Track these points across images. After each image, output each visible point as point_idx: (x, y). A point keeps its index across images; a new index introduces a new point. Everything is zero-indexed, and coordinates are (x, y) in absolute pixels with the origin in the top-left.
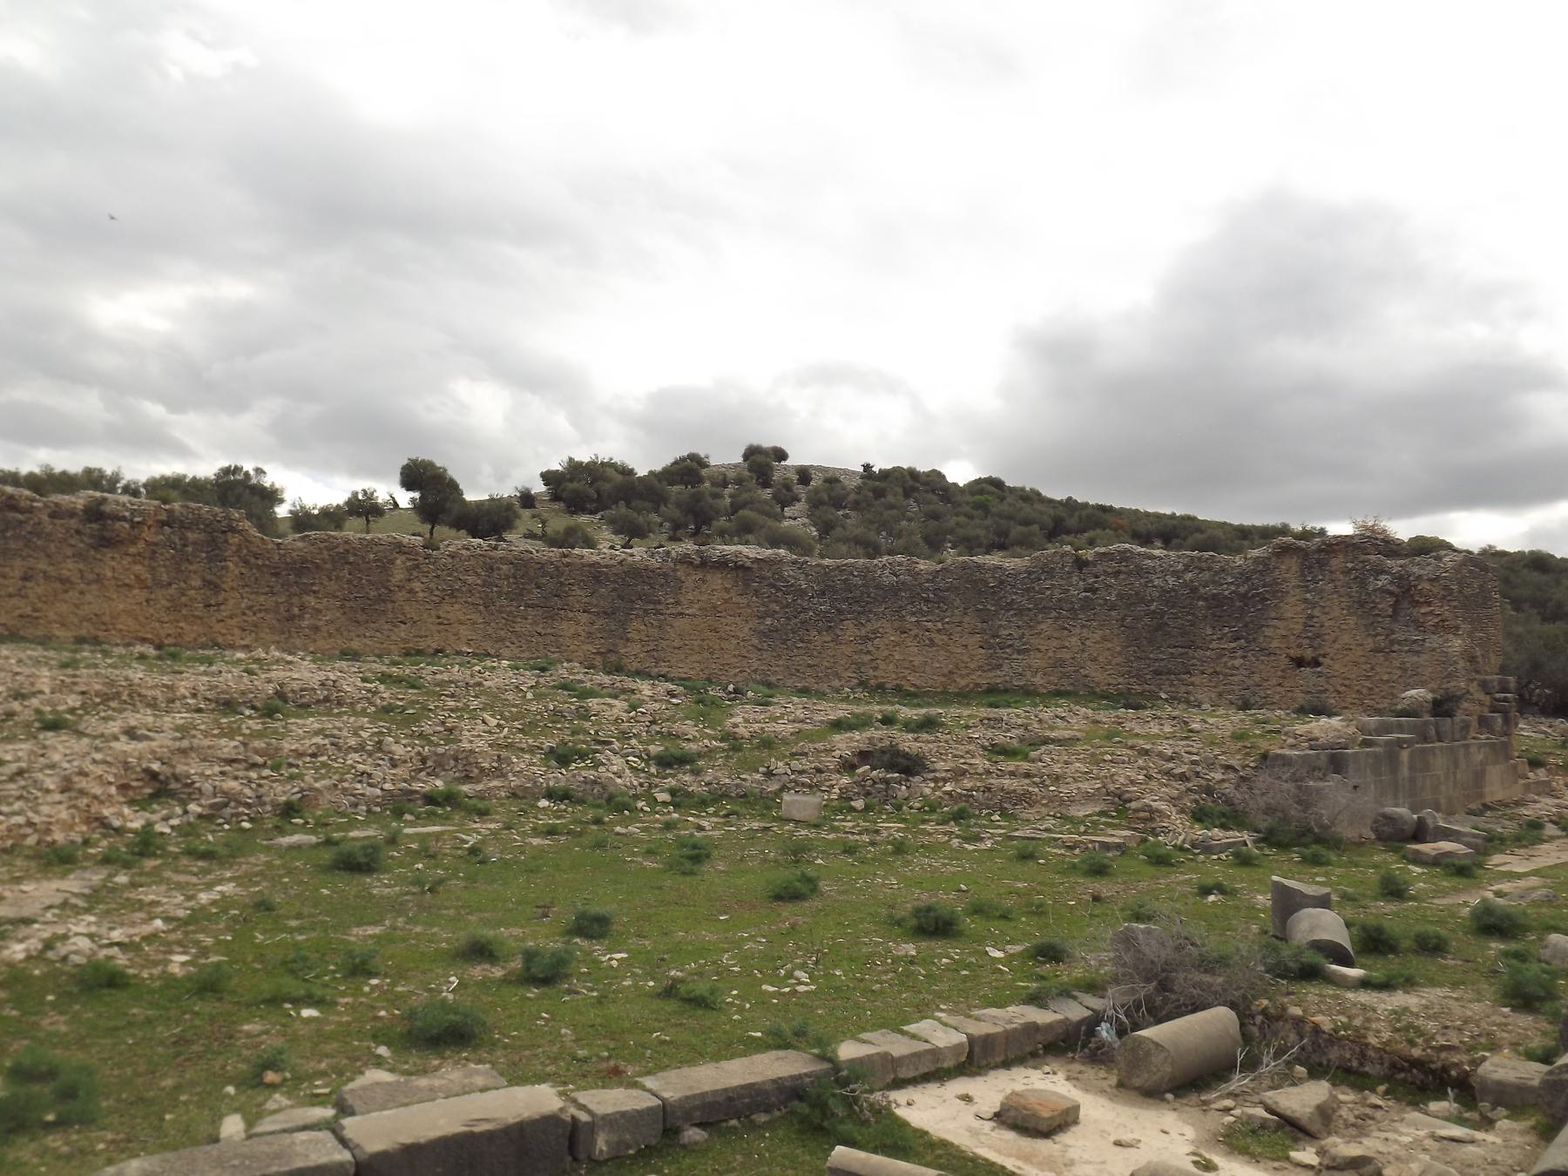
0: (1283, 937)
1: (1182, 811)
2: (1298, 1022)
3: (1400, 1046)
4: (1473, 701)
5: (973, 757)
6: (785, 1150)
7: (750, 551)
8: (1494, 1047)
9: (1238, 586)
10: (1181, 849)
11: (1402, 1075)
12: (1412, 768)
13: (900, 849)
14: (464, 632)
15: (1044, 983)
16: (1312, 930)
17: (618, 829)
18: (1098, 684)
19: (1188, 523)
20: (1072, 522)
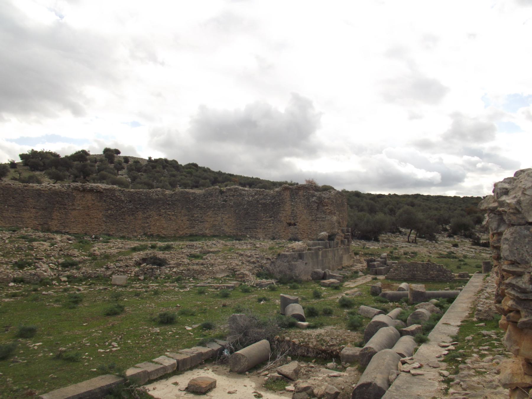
0: (284, 314)
1: (253, 274)
2: (289, 342)
7: (102, 186)
8: (346, 343)
10: (253, 286)
12: (322, 257)
13: (156, 293)
15: (205, 338)
16: (293, 310)
17: (44, 292)
18: (227, 232)
20: (220, 179)
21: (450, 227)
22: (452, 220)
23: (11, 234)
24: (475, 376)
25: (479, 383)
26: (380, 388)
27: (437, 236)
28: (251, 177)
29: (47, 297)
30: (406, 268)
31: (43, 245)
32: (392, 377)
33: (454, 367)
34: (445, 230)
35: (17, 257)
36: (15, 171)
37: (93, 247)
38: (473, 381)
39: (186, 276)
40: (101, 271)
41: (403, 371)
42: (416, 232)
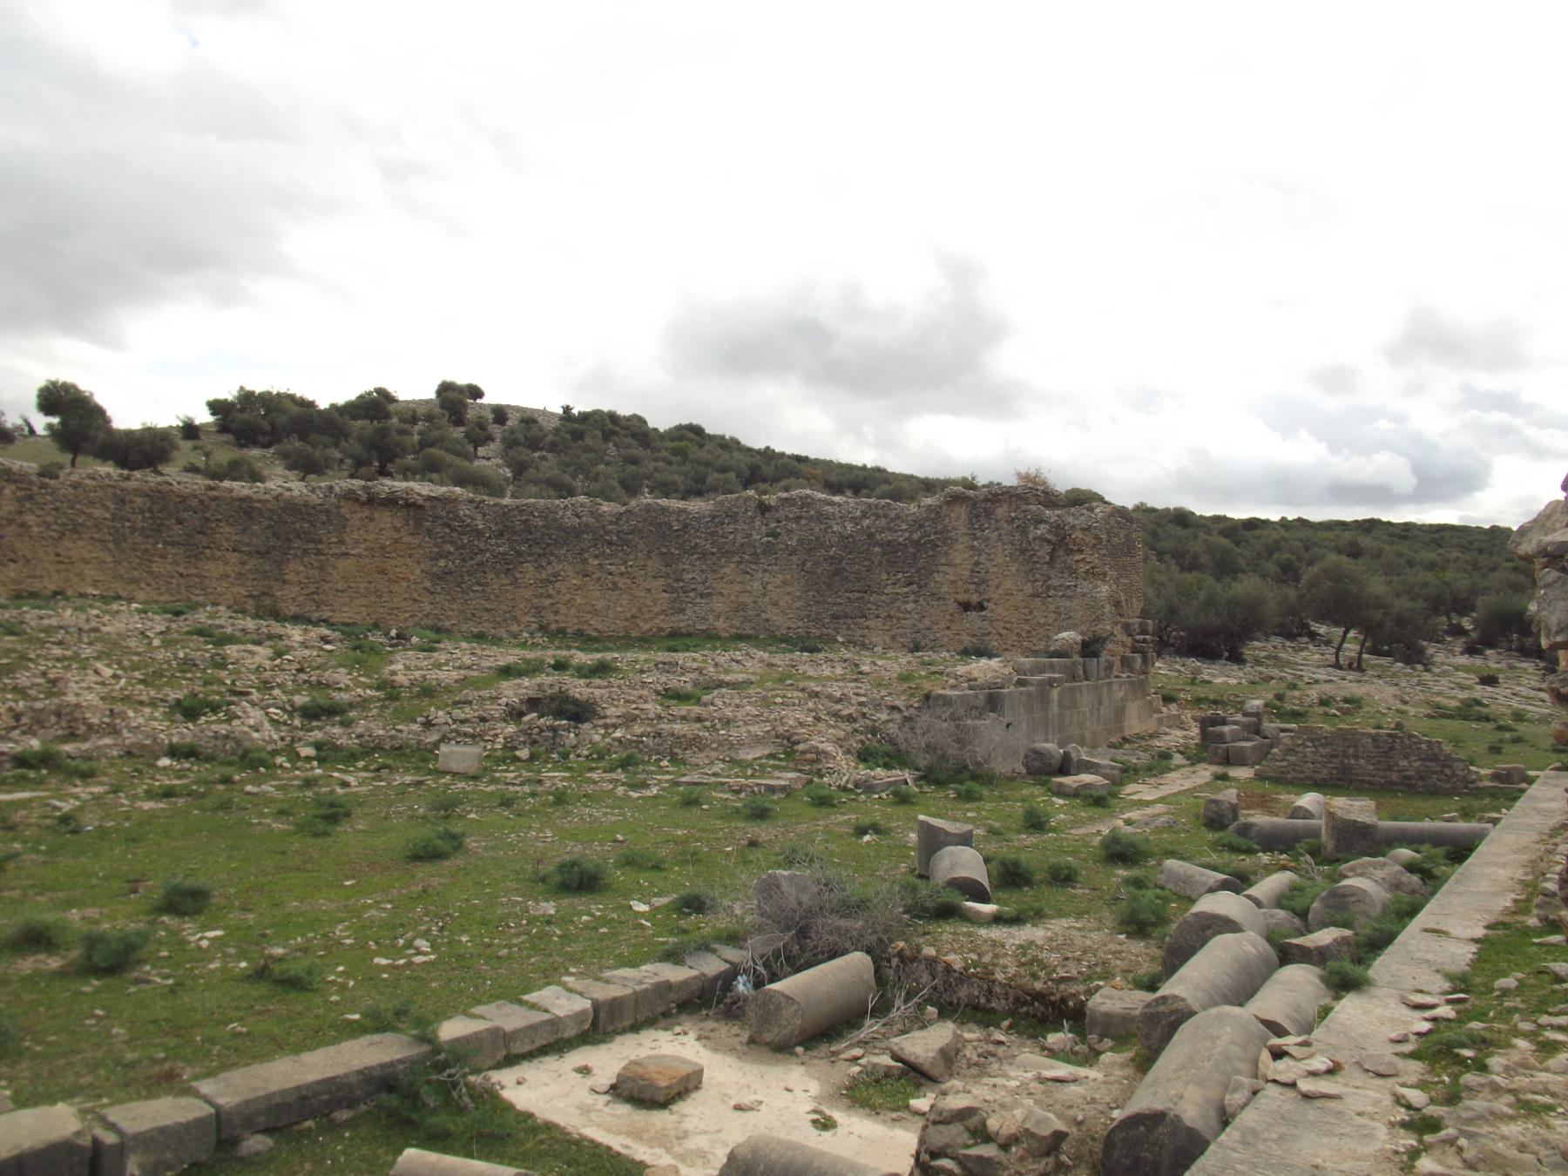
1: (848, 752)
2: (932, 962)
3: (1024, 981)
4: (1116, 642)
5: (646, 702)
6: (365, 1151)
7: (421, 488)
8: (1107, 976)
9: (912, 533)
10: (844, 789)
11: (1025, 1009)
12: (1061, 705)
13: (560, 799)
14: (90, 572)
15: (685, 938)
16: (952, 867)
17: (249, 788)
18: (778, 628)
19: (877, 475)
20: (768, 470)
21: (1475, 622)
22: (1481, 601)
23: (171, 621)
24: (1512, 1118)
25: (1522, 1148)
26: (1191, 1132)
27: (1431, 651)
28: (860, 464)
29: (256, 800)
30: (1323, 746)
31: (252, 653)
32: (1237, 1098)
33: (1446, 1079)
34: (1458, 631)
35: (180, 687)
36: (195, 448)
37: (391, 663)
38: (1503, 1138)
39: (651, 752)
40: (409, 731)
41: (1275, 1081)
42: (1361, 637)
